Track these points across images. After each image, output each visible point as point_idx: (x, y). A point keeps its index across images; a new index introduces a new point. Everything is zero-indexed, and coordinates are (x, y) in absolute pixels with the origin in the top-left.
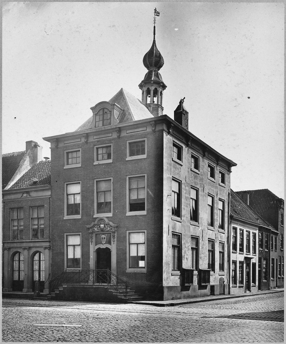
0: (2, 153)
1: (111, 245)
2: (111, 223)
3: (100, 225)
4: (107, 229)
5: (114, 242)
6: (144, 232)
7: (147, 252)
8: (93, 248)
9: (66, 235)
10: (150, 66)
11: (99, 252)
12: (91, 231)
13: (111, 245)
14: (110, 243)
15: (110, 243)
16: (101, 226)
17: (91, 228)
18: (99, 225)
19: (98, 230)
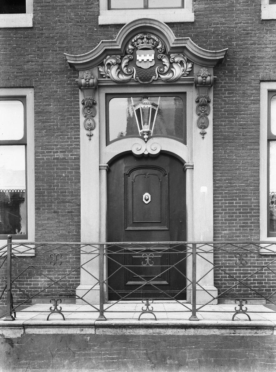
0: (98, 24)
1: (185, 143)
2: (191, 45)
3: (134, 53)
4: (170, 71)
5: (203, 126)
6: (22, 99)
7: (270, 118)
8: (91, 158)
9: (25, 97)
10: (214, 77)
11: (123, 169)
12: (84, 78)
13: (185, 143)
14: (180, 134)
15: (180, 134)
16: (139, 58)
17: (88, 66)
18: (125, 53)
19: (122, 77)
